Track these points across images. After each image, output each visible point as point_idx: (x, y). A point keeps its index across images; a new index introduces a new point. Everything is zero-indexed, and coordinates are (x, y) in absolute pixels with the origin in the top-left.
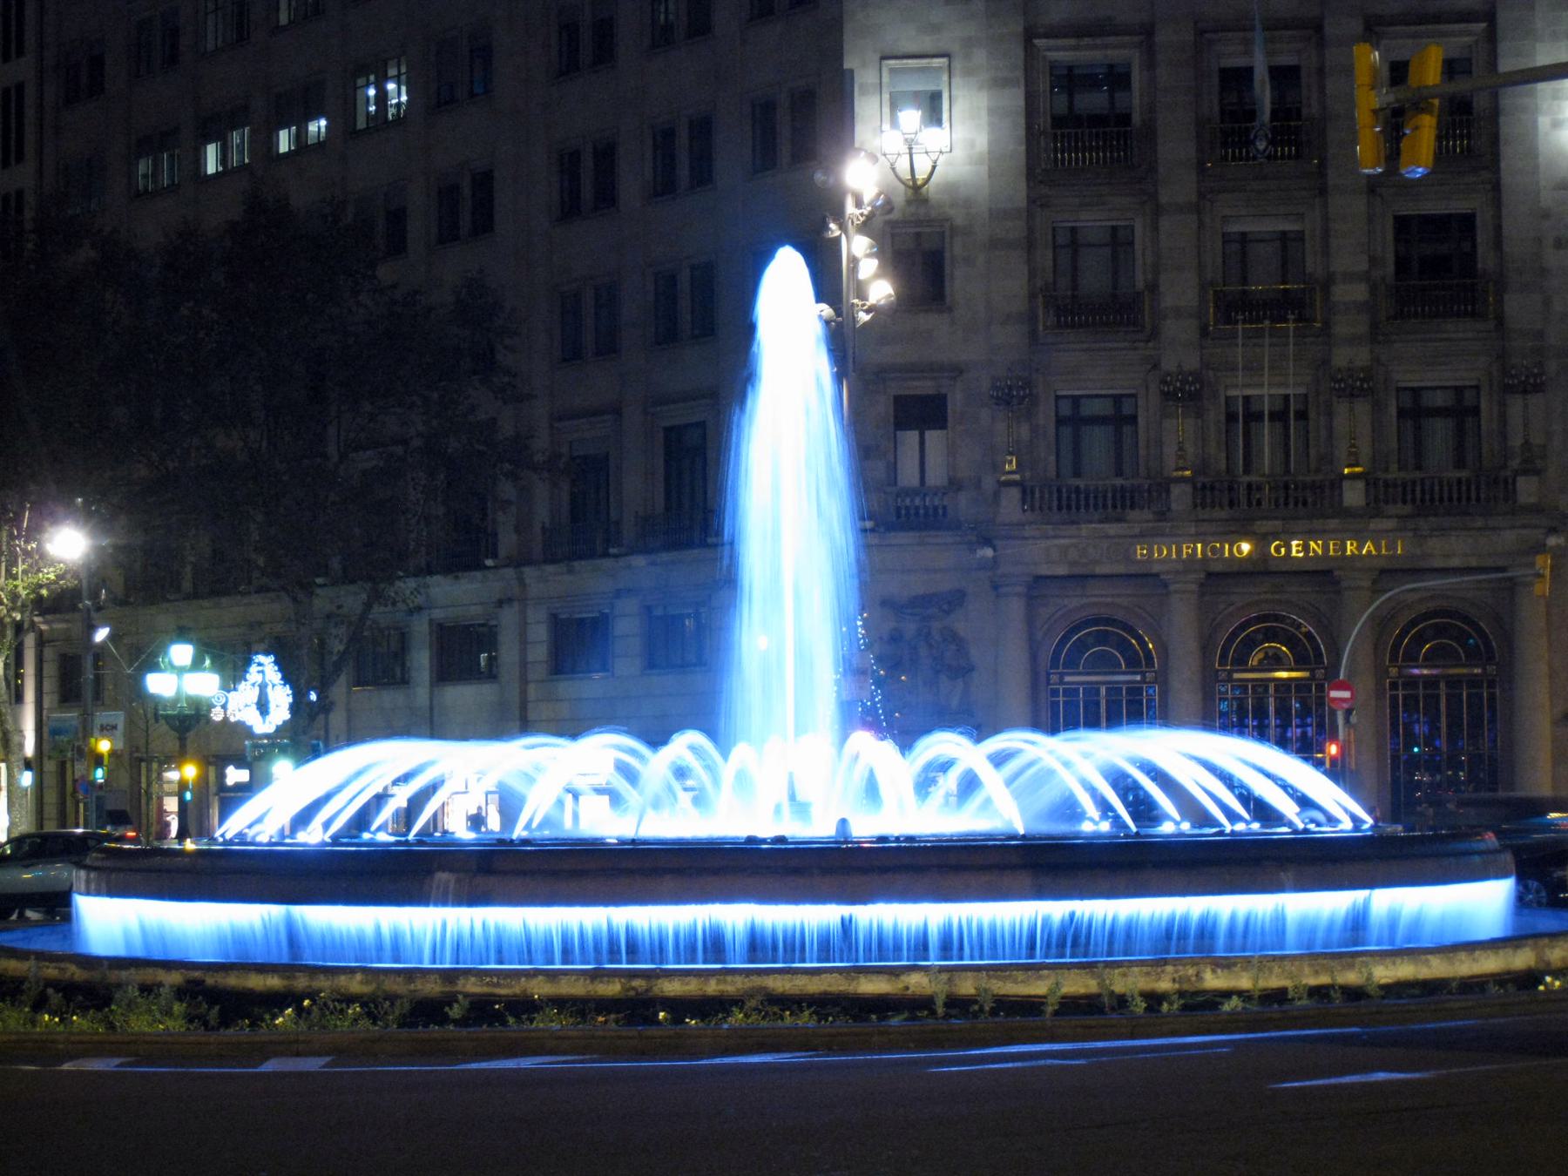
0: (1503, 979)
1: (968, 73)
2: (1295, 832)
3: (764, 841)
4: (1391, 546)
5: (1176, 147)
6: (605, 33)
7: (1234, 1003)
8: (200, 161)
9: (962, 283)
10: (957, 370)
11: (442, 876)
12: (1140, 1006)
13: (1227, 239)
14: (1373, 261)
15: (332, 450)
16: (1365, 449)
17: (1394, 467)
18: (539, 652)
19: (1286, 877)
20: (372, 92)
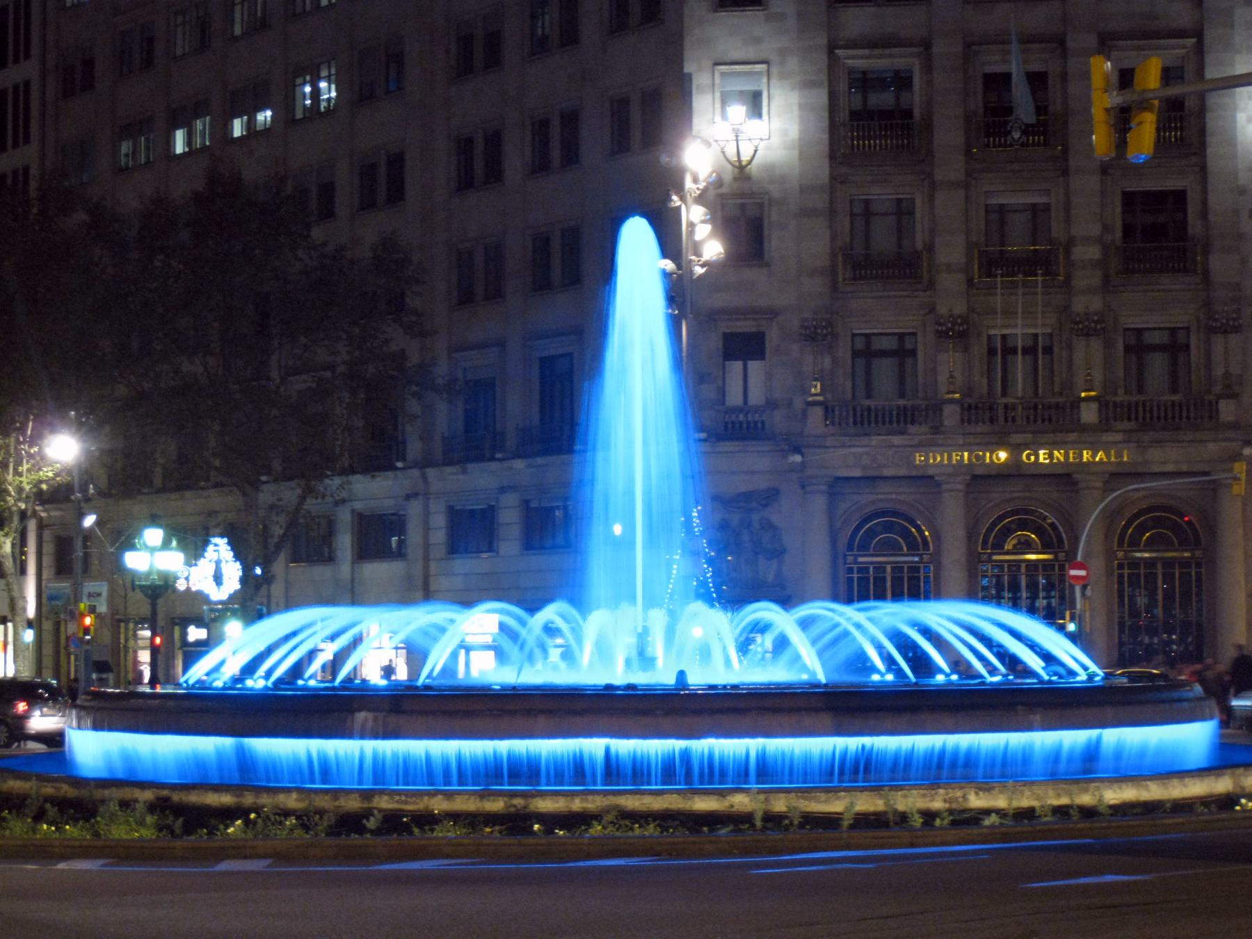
0: (1206, 801)
1: (783, 76)
2: (1041, 681)
3: (618, 688)
4: (1119, 455)
5: (948, 135)
6: (494, 42)
7: (994, 819)
8: (170, 142)
9: (778, 243)
10: (772, 313)
11: (361, 716)
12: (918, 821)
13: (988, 209)
14: (1106, 228)
15: (275, 374)
16: (1098, 375)
17: (1121, 391)
18: (439, 536)
19: (1037, 718)
20: (308, 89)
